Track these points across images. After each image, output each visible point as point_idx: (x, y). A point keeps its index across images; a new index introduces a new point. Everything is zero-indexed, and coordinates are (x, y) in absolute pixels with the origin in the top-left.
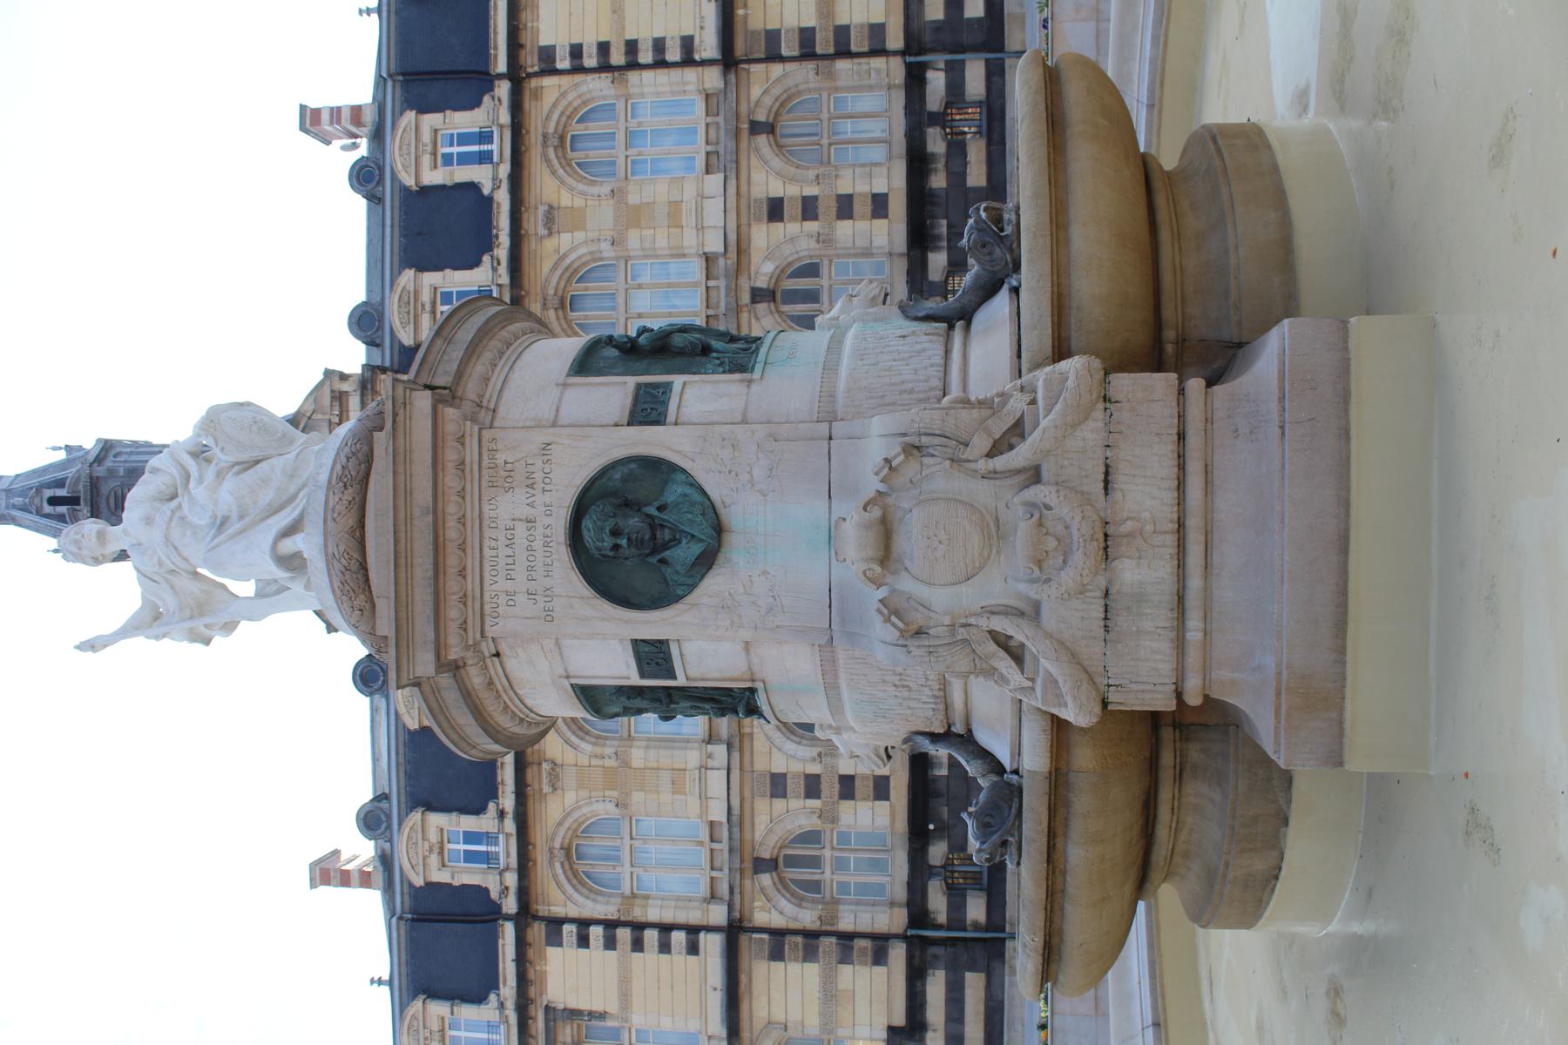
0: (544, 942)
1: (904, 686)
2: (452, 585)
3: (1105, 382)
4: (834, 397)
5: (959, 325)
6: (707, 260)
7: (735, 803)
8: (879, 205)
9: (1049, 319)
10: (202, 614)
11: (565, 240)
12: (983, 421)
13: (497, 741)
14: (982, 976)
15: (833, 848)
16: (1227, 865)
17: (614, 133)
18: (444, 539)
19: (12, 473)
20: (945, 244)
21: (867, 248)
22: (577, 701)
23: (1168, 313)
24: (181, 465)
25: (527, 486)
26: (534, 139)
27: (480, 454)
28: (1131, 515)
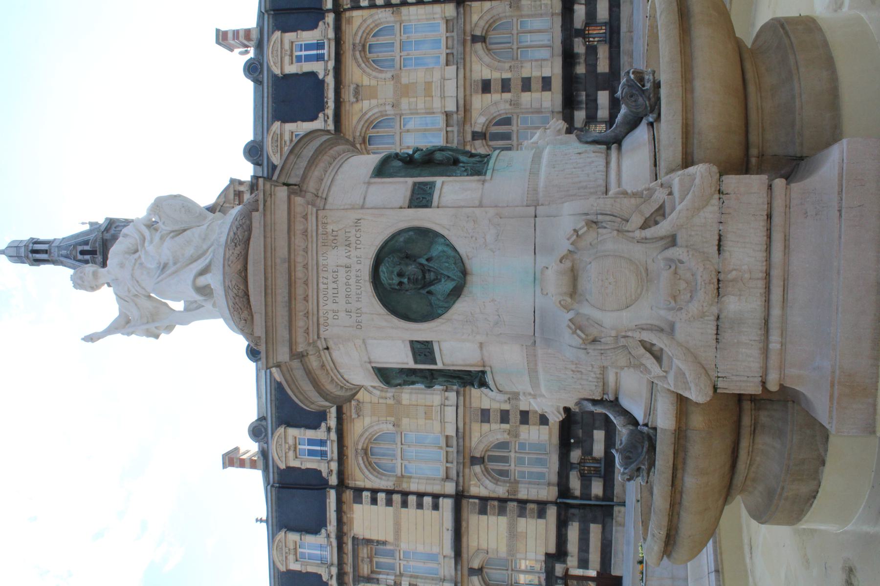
0: (352, 501)
1: (578, 371)
2: (300, 306)
3: (719, 180)
5: (614, 146)
6: (447, 115)
7: (461, 425)
8: (546, 84)
9: (680, 141)
10: (153, 321)
11: (366, 104)
13: (327, 400)
14: (600, 526)
16: (783, 488)
17: (394, 43)
18: (295, 278)
19: (61, 237)
20: (584, 106)
22: (376, 377)
23: (753, 138)
24: (140, 232)
25: (346, 245)
26: (347, 46)
27: (317, 226)
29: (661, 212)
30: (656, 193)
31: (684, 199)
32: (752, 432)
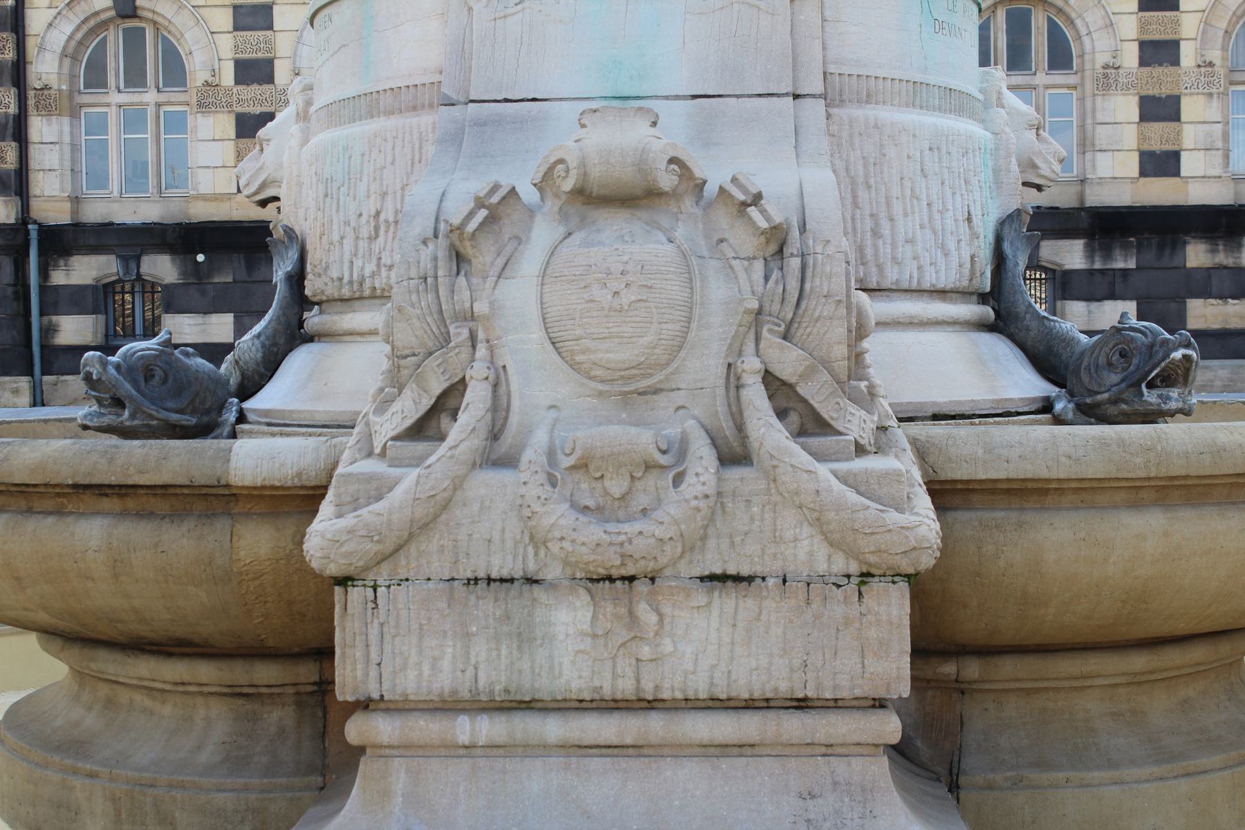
1: (377, 228)
3: (896, 575)
4: (867, 102)
5: (988, 312)
9: (1002, 475)
12: (826, 363)
15: (159, 105)
16: (92, 775)
20: (1098, 265)
21: (1093, 145)
23: (1008, 667)
28: (667, 621)
29: (810, 426)
30: (863, 413)
31: (846, 483)
32: (238, 690)
